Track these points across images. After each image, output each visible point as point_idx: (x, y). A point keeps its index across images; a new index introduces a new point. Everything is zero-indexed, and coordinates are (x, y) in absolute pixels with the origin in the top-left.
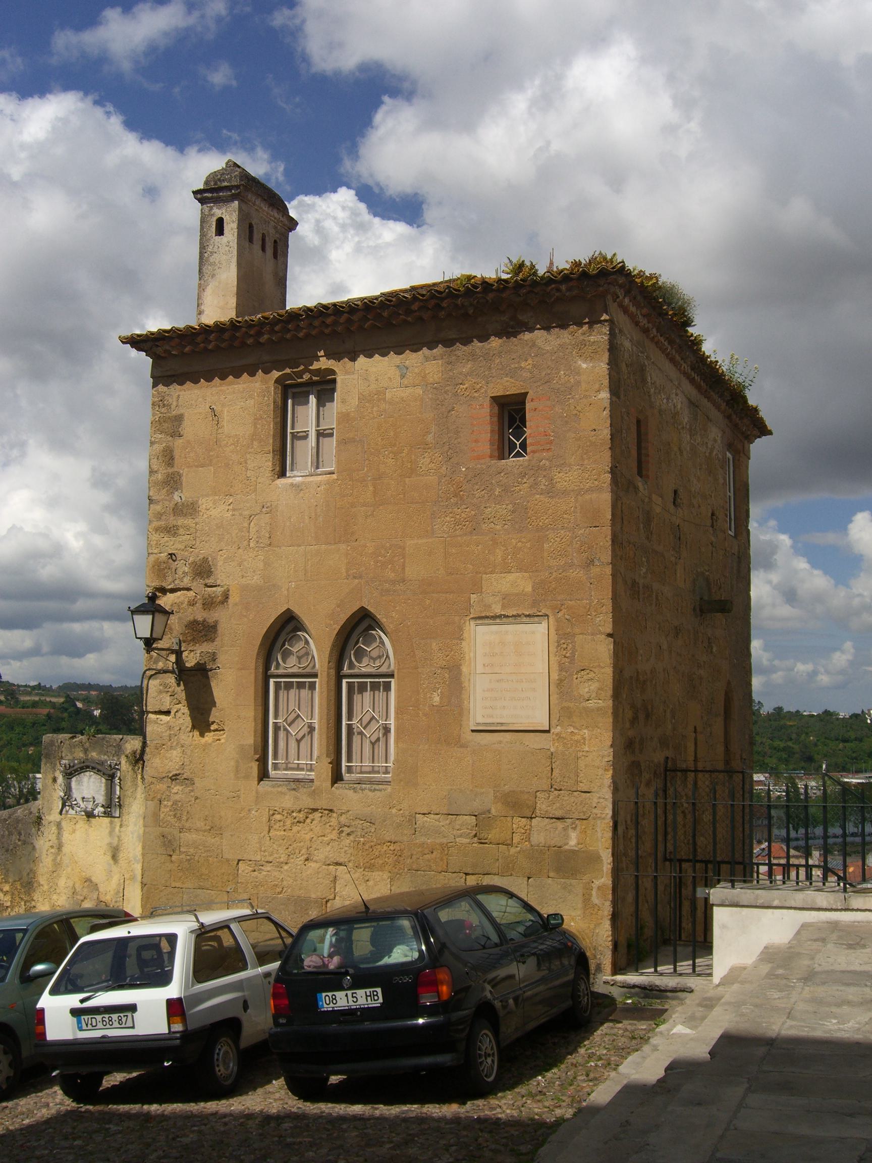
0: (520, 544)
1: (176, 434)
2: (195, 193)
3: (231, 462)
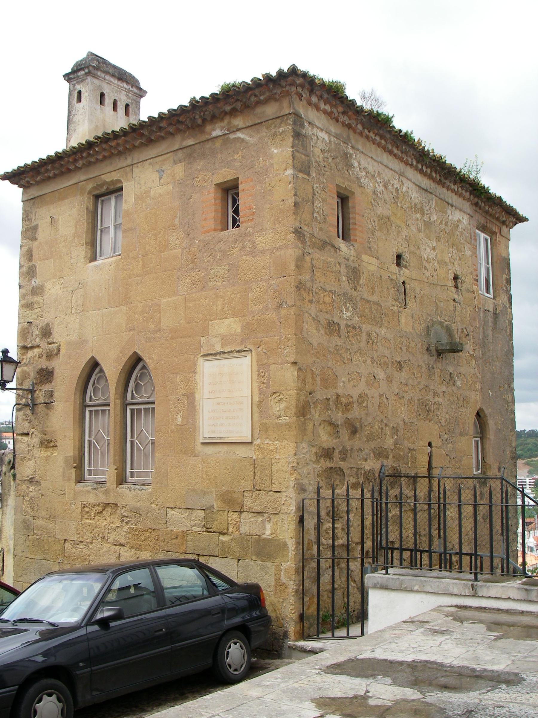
1: (34, 239)
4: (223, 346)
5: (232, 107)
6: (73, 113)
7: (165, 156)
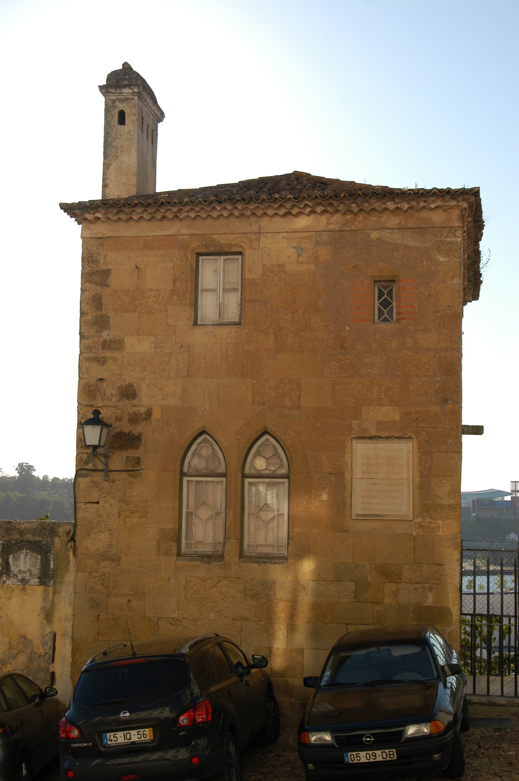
0: (391, 385)
1: (103, 284)
2: (101, 88)
3: (153, 311)
4: (377, 430)
5: (396, 206)
6: (113, 134)
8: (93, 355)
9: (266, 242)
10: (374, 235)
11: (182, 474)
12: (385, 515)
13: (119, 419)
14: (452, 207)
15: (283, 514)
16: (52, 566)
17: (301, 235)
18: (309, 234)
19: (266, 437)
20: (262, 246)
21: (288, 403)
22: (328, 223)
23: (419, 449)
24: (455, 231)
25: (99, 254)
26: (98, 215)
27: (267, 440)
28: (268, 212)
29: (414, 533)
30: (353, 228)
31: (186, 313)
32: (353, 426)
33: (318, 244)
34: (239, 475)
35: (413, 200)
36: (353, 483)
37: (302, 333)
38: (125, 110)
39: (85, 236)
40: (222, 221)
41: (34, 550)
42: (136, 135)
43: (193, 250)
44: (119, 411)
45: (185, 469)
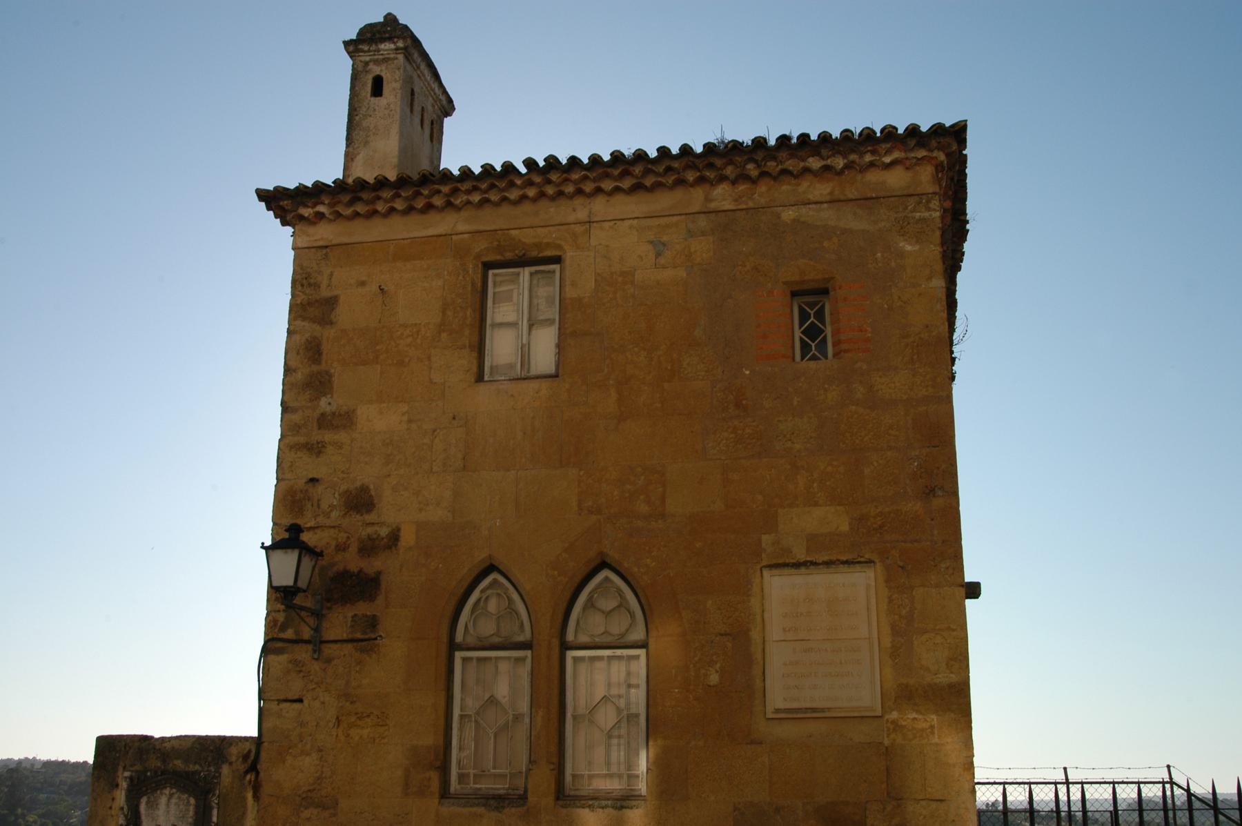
0: (830, 469)
1: (325, 320)
2: (347, 44)
3: (407, 360)
4: (808, 550)
7: (666, 219)
8: (302, 440)
9: (599, 236)
10: (788, 215)
11: (453, 646)
12: (829, 709)
13: (341, 548)
14: (920, 161)
15: (637, 715)
16: (215, 819)
17: (663, 221)
18: (675, 219)
19: (605, 573)
20: (593, 242)
21: (643, 508)
22: (708, 199)
23: (887, 581)
24: (928, 201)
25: (320, 273)
26: (321, 208)
27: (607, 579)
28: (603, 186)
29: (887, 742)
30: (751, 205)
31: (466, 360)
32: (764, 545)
33: (691, 234)
34: (556, 642)
35: (853, 151)
36: (767, 650)
37: (666, 385)
38: (383, 74)
39: (300, 245)
40: (527, 207)
41: (183, 789)
42: (398, 110)
43: (478, 257)
44: (342, 534)
45: (459, 637)
